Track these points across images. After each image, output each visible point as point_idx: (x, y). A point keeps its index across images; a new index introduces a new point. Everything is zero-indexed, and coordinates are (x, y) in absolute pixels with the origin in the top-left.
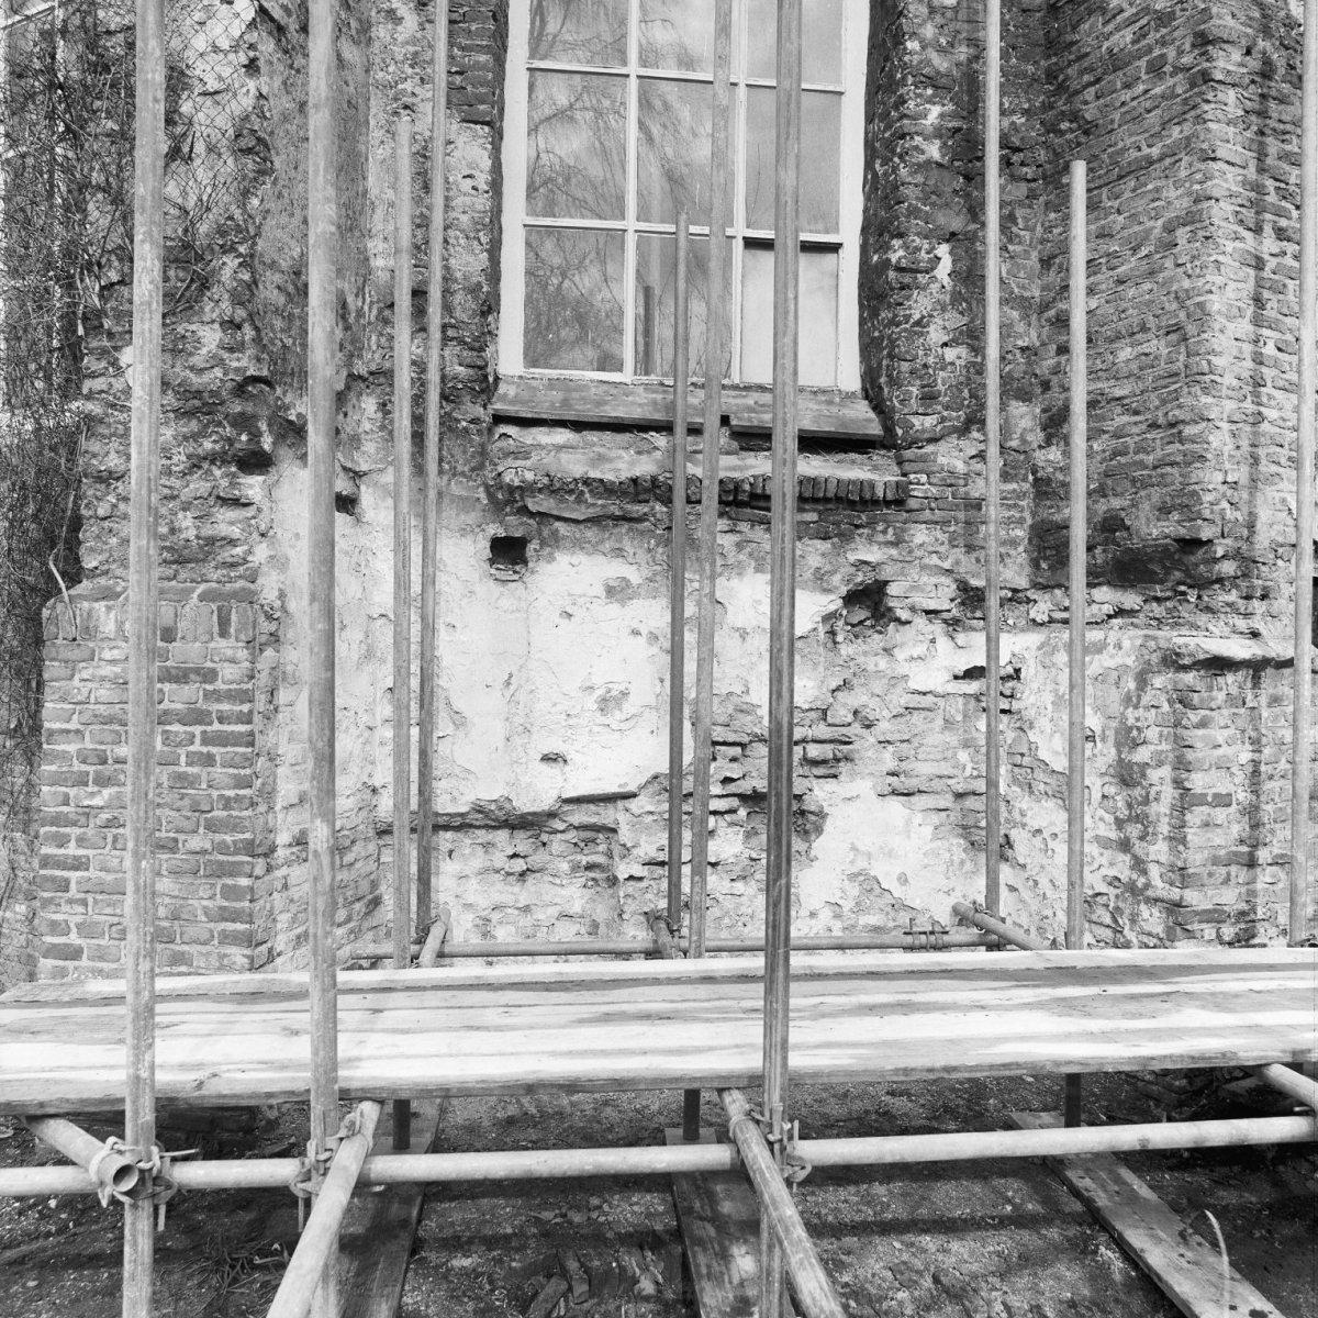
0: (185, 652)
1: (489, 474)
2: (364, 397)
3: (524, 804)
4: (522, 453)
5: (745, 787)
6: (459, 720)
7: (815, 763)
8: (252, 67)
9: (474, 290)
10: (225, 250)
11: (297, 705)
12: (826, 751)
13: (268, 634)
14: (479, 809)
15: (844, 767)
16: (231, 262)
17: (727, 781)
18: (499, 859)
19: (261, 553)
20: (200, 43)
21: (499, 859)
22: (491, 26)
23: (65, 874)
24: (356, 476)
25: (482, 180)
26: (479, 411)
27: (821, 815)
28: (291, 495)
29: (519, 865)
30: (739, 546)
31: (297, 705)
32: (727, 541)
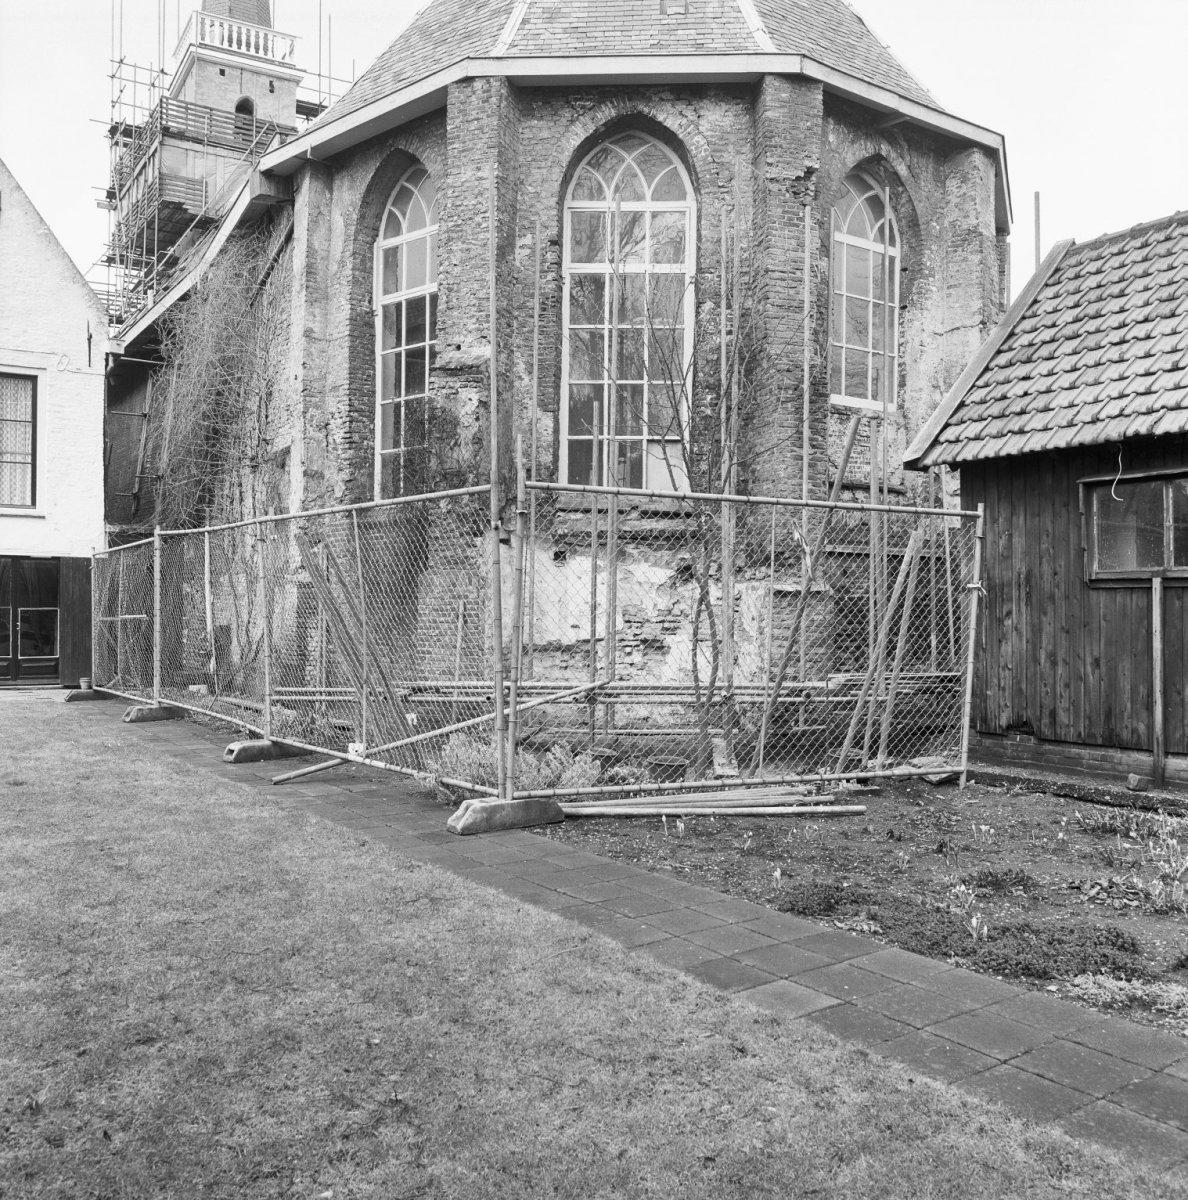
0: (460, 589)
1: (552, 529)
2: (948, 183)
3: (565, 642)
4: (564, 522)
5: (642, 637)
6: (543, 613)
7: (667, 629)
8: (477, 419)
9: (548, 468)
10: (471, 472)
11: (491, 605)
12: (672, 625)
13: (482, 584)
14: (550, 644)
15: (678, 631)
16: (471, 476)
17: (635, 635)
18: (558, 662)
19: (480, 560)
20: (463, 412)
21: (558, 662)
22: (553, 379)
23: (567, 281)
24: (509, 532)
25: (550, 431)
26: (550, 509)
27: (669, 647)
28: (488, 542)
29: (564, 664)
30: (640, 553)
31: (491, 605)
32: (635, 552)
